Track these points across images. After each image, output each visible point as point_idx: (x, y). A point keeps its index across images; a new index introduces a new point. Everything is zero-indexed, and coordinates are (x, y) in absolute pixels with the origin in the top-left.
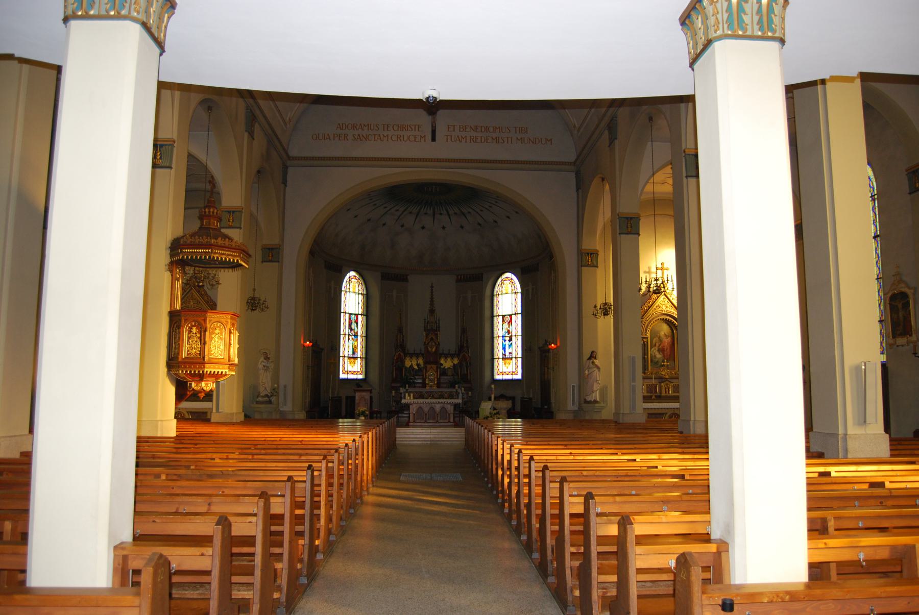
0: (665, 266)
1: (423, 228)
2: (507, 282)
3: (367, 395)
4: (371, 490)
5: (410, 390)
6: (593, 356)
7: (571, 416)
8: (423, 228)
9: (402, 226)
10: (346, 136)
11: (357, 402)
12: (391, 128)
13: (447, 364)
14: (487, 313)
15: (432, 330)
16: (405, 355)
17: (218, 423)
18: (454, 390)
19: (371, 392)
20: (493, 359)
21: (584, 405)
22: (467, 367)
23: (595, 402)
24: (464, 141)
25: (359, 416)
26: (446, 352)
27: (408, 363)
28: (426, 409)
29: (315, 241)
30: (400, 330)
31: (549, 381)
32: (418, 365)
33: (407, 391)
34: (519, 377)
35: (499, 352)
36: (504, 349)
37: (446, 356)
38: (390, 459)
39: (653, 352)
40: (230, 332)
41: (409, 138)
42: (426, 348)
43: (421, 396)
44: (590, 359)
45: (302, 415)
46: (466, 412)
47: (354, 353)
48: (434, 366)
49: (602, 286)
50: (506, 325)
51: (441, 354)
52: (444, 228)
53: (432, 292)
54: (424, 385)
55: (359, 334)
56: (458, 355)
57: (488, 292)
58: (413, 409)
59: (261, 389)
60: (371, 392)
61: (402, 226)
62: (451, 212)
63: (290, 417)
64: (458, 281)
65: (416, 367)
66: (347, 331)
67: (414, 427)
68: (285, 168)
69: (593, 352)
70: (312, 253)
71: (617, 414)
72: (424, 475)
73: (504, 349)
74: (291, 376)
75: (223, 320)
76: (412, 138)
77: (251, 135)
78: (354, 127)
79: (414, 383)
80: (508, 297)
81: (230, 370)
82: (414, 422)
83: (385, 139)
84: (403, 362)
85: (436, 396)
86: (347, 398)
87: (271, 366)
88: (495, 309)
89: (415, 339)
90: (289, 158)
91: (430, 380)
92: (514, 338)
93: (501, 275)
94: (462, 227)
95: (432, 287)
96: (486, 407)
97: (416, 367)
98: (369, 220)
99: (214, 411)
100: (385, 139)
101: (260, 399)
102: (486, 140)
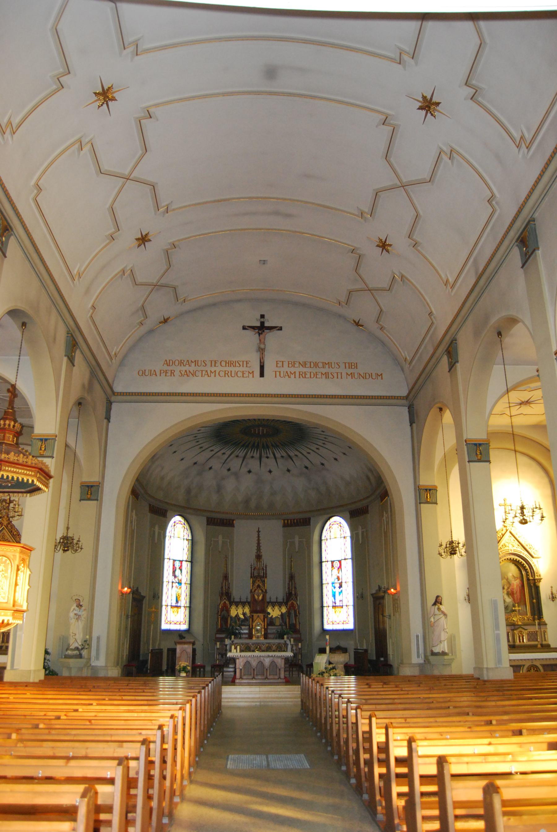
0: (503, 502)
1: (250, 472)
2: (335, 527)
3: (189, 648)
4: (187, 792)
5: (236, 641)
6: (438, 601)
7: (416, 672)
9: (229, 470)
10: (172, 373)
11: (178, 655)
12: (218, 364)
13: (275, 612)
14: (315, 559)
15: (259, 576)
16: (231, 603)
17: (15, 685)
18: (282, 641)
19: (193, 644)
20: (322, 607)
21: (432, 658)
22: (296, 616)
23: (444, 654)
25: (180, 672)
26: (273, 600)
27: (234, 612)
28: (254, 664)
29: (137, 480)
30: (226, 577)
31: (385, 631)
32: (244, 614)
33: (233, 643)
35: (328, 600)
36: (334, 596)
37: (273, 604)
38: (215, 731)
40: (18, 569)
41: (237, 374)
42: (253, 596)
43: (247, 648)
44: (435, 604)
45: (115, 672)
46: (297, 668)
47: (177, 602)
48: (261, 615)
49: (450, 520)
50: (335, 571)
51: (268, 603)
52: (270, 472)
53: (259, 536)
54: (250, 636)
55: (183, 582)
56: (286, 604)
57: (316, 537)
58: (240, 664)
59: (71, 641)
60: (193, 644)
61: (229, 470)
62: (278, 455)
63: (102, 674)
64: (285, 526)
65: (242, 616)
66: (171, 578)
67: (241, 684)
68: (109, 404)
69: (438, 597)
70: (134, 493)
71: (478, 668)
72: (258, 758)
73: (334, 596)
74: (104, 626)
75: (9, 554)
76: (240, 374)
78: (181, 363)
79: (240, 633)
80: (336, 540)
81: (14, 618)
82: (241, 678)
83: (213, 375)
84: (228, 611)
85: (263, 648)
86: (169, 650)
87: (83, 613)
89: (241, 586)
90: (114, 393)
91: (257, 630)
92: (343, 584)
93: (329, 519)
94: (288, 471)
95: (259, 532)
96: (321, 661)
97: (242, 616)
98: (195, 463)
99: (8, 667)
100: (213, 375)
101: (69, 652)
102: (316, 375)
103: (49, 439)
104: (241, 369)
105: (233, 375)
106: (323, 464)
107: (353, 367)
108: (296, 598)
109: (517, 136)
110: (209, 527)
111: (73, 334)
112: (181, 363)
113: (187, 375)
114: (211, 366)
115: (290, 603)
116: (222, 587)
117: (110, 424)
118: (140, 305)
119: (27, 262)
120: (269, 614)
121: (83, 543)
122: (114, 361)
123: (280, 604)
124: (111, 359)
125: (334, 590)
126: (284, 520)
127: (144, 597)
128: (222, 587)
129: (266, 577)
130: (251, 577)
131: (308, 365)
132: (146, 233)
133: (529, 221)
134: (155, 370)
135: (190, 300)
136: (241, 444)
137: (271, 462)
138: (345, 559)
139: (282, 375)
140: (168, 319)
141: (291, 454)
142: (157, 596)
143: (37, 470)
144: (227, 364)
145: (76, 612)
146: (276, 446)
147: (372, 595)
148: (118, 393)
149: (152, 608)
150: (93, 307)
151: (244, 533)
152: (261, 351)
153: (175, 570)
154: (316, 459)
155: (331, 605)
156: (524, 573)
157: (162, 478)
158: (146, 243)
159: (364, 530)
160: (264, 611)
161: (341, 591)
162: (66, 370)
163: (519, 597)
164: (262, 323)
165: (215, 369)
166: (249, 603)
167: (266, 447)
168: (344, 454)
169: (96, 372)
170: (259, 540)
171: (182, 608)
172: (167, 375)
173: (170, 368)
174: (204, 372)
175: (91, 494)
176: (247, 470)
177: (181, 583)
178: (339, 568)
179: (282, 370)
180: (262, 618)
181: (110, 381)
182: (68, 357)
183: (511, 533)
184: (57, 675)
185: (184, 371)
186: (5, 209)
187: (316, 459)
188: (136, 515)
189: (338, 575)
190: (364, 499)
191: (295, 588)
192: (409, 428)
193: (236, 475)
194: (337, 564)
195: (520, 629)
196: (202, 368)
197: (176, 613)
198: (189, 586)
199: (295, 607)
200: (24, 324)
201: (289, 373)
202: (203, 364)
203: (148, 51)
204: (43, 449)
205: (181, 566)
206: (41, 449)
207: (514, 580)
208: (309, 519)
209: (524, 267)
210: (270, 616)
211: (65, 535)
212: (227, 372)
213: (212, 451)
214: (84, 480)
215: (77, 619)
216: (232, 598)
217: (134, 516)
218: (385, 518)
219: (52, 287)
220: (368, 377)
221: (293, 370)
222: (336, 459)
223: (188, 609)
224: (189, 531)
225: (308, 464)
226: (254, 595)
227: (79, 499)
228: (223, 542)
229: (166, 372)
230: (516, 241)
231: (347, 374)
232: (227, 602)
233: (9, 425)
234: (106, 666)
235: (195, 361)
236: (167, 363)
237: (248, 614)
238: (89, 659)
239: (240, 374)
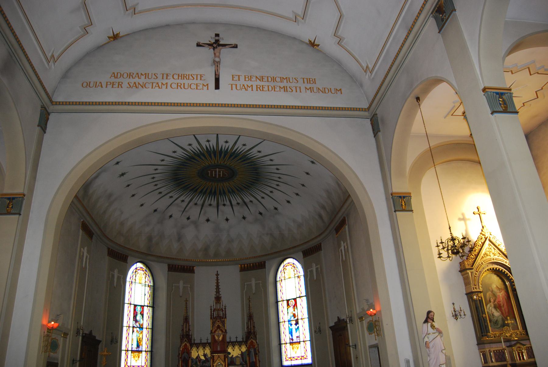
1: (208, 220)
2: (289, 268)
6: (429, 318)
8: (208, 220)
9: (188, 218)
10: (120, 85)
13: (235, 352)
14: (271, 299)
15: (218, 318)
16: (192, 345)
22: (256, 354)
24: (250, 89)
26: (233, 339)
29: (76, 197)
30: (186, 320)
32: (205, 355)
34: (309, 361)
35: (285, 337)
37: (233, 344)
39: (490, 309)
42: (213, 337)
44: (426, 321)
47: (138, 346)
48: (222, 355)
50: (291, 309)
51: (229, 343)
52: (227, 220)
53: (217, 280)
55: (145, 326)
57: (271, 279)
62: (234, 202)
64: (243, 269)
65: (203, 358)
66: (132, 323)
69: (429, 312)
76: (193, 86)
78: (130, 75)
80: (290, 280)
84: (189, 353)
88: (279, 294)
89: (202, 328)
92: (300, 321)
93: (283, 261)
94: (244, 218)
95: (217, 275)
97: (203, 358)
98: (155, 211)
102: (274, 88)
103: (17, 198)
104: (195, 81)
105: (186, 87)
106: (276, 209)
107: (311, 82)
108: (256, 336)
109: (364, 66)
110: (170, 273)
112: (130, 75)
113: (136, 86)
114: (163, 78)
115: (249, 342)
116: (183, 330)
117: (46, 136)
120: (230, 353)
123: (240, 344)
125: (290, 327)
126: (241, 265)
127: (99, 342)
128: (183, 330)
129: (226, 317)
130: (211, 318)
131: (266, 79)
133: (374, 115)
134: (101, 83)
136: (199, 190)
137: (227, 210)
138: (300, 297)
139: (238, 88)
141: (247, 200)
142: (115, 340)
144: (180, 77)
146: (232, 192)
147: (331, 328)
148: (56, 102)
151: (204, 279)
152: (216, 64)
153: (137, 315)
154: (269, 203)
155: (288, 341)
156: (507, 283)
157: (122, 224)
159: (319, 266)
160: (224, 351)
161: (298, 327)
163: (507, 311)
164: (217, 41)
166: (209, 344)
167: (223, 193)
168: (297, 194)
170: (218, 283)
171: (144, 353)
174: (154, 85)
176: (206, 218)
177: (142, 328)
178: (294, 306)
179: (238, 83)
180: (223, 358)
181: (50, 94)
183: (490, 240)
187: (269, 203)
188: (88, 252)
189: (294, 312)
190: (316, 237)
191: (254, 327)
192: (373, 140)
193: (195, 223)
194: (292, 303)
195: (518, 345)
196: (152, 80)
197: (137, 358)
198: (150, 331)
199: (255, 346)
201: (246, 87)
202: (154, 76)
203: (140, 12)
205: (143, 311)
207: (498, 291)
208: (265, 262)
209: (441, 32)
210: (230, 356)
212: (179, 84)
213: (171, 197)
216: (193, 339)
217: (85, 254)
218: (343, 248)
220: (327, 91)
221: (250, 83)
222: (288, 202)
223: (149, 354)
224: (151, 278)
225: (262, 210)
226: (214, 336)
228: (184, 287)
229: (113, 84)
230: (432, 13)
231: (306, 88)
232: (188, 344)
236: (115, 76)
237: (209, 355)
239: (193, 86)
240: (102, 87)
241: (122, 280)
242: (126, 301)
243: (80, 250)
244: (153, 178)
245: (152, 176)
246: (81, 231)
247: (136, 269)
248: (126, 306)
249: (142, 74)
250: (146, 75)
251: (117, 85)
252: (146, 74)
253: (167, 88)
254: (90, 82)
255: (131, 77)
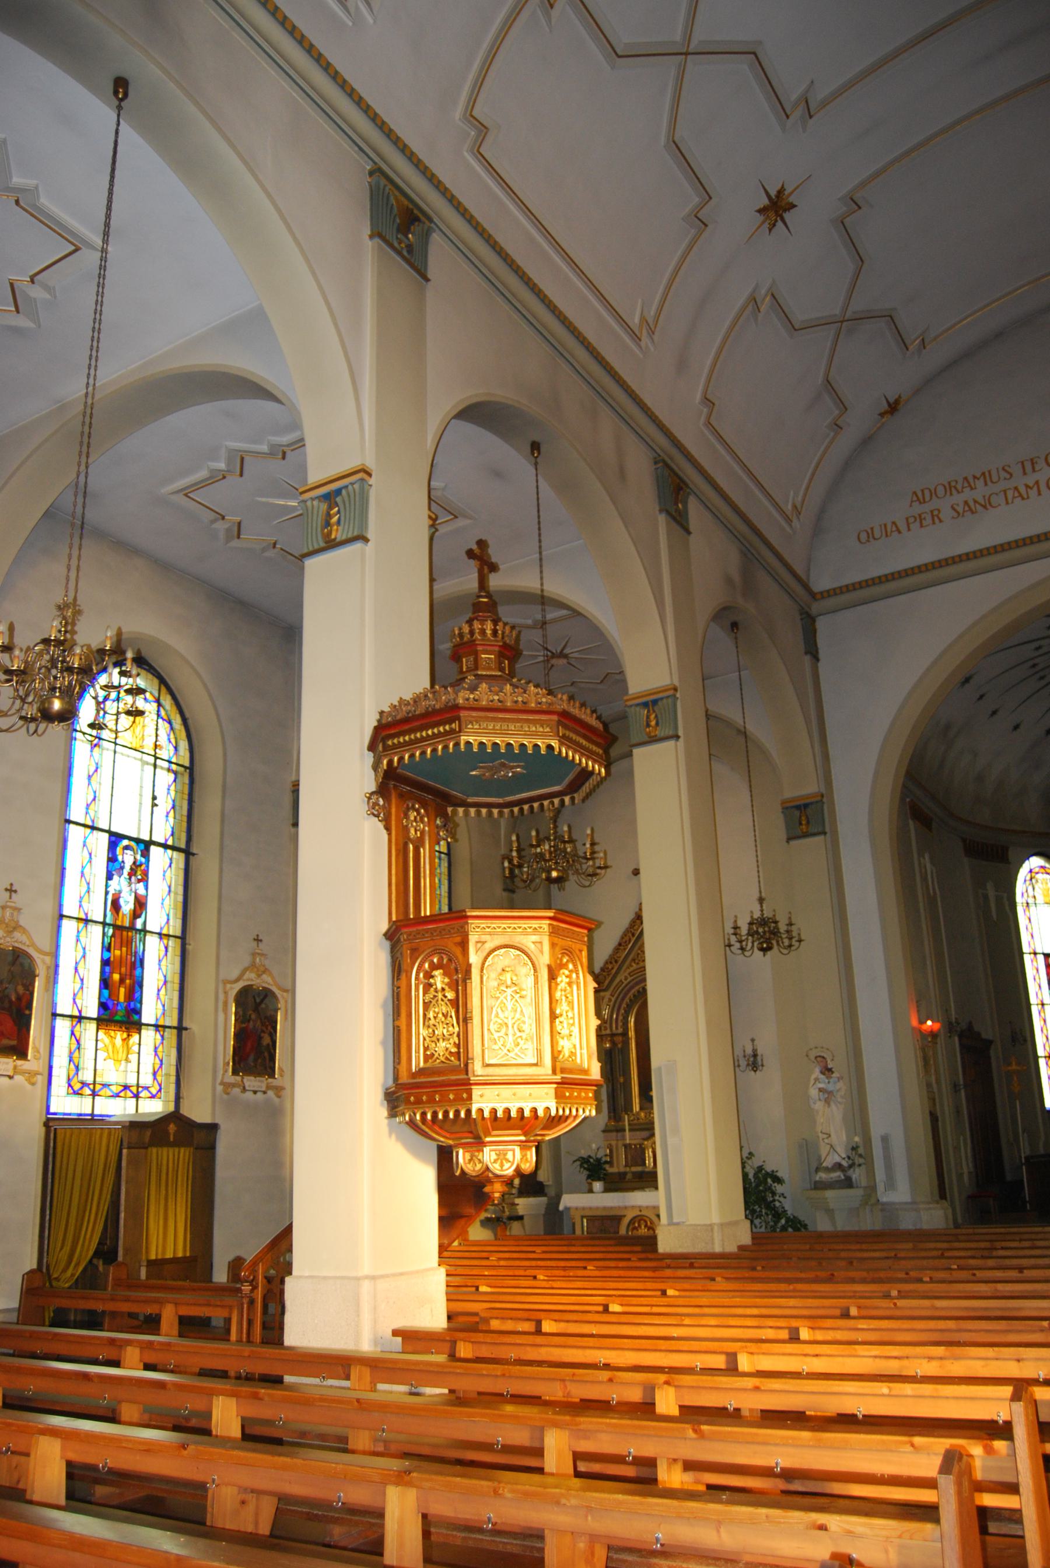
59: (824, 1150)
63: (907, 1223)
77: (679, 520)
78: (950, 488)
83: (1033, 493)
87: (840, 1087)
90: (813, 595)
100: (1033, 493)
101: (822, 1176)
103: (812, 803)
111: (669, 462)
112: (950, 488)
113: (970, 509)
114: (1025, 473)
117: (819, 664)
118: (820, 379)
119: (499, 299)
121: (803, 926)
122: (795, 523)
124: (789, 520)
127: (989, 1043)
132: (779, 187)
134: (894, 523)
135: (935, 338)
140: (897, 402)
143: (555, 718)
145: (821, 1086)
148: (821, 593)
149: (1010, 1064)
150: (707, 401)
158: (786, 216)
162: (670, 547)
165: (1036, 476)
169: (754, 549)
172: (924, 523)
173: (927, 508)
174: (1010, 494)
175: (808, 823)
182: (668, 513)
184: (805, 1226)
185: (962, 505)
186: (395, 172)
200: (535, 446)
202: (1003, 474)
204: (653, 723)
206: (648, 725)
211: (757, 915)
214: (788, 794)
215: (827, 1102)
217: (928, 866)
219: (582, 354)
227: (784, 837)
229: (921, 518)
233: (483, 632)
234: (913, 1203)
235: (983, 474)
236: (919, 498)
238: (872, 1188)
240: (900, 532)
241: (1006, 903)
242: (1025, 948)
243: (920, 864)
244: (1034, 666)
245: (1031, 663)
246: (911, 822)
247: (1031, 871)
248: (1027, 958)
249: (975, 477)
250: (986, 477)
251: (929, 520)
252: (983, 474)
253: (1039, 494)
254: (872, 529)
255: (954, 491)
